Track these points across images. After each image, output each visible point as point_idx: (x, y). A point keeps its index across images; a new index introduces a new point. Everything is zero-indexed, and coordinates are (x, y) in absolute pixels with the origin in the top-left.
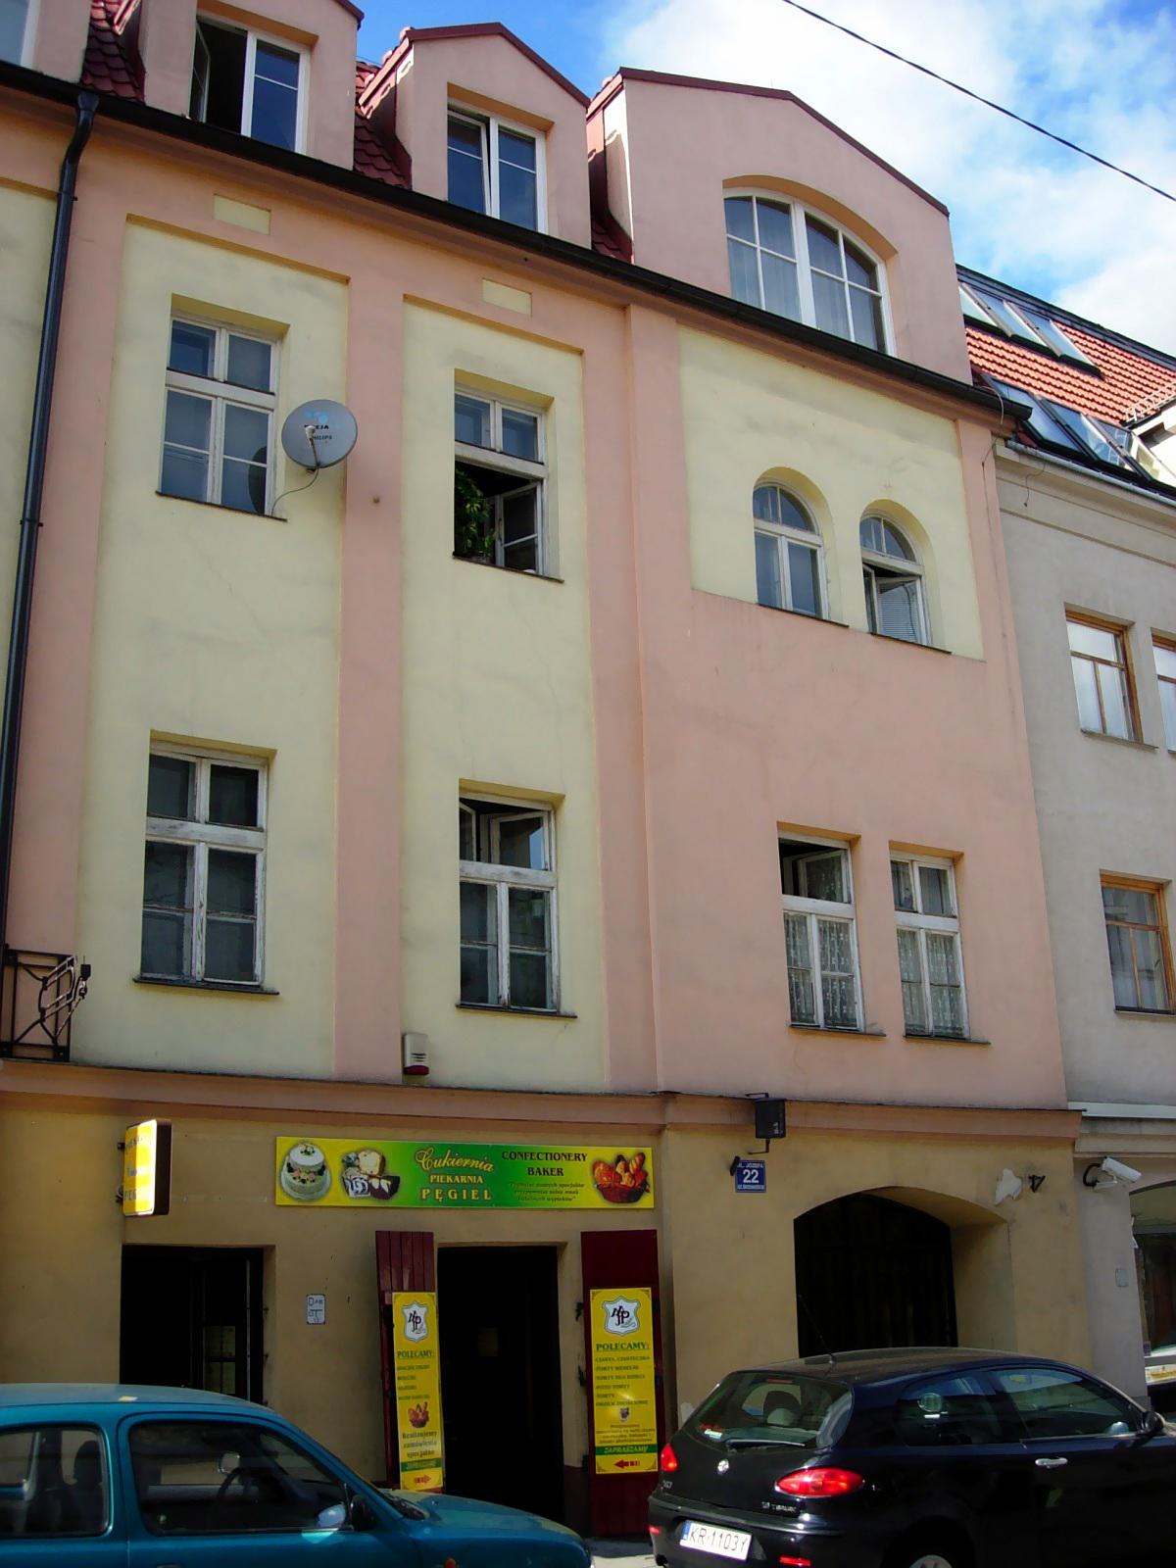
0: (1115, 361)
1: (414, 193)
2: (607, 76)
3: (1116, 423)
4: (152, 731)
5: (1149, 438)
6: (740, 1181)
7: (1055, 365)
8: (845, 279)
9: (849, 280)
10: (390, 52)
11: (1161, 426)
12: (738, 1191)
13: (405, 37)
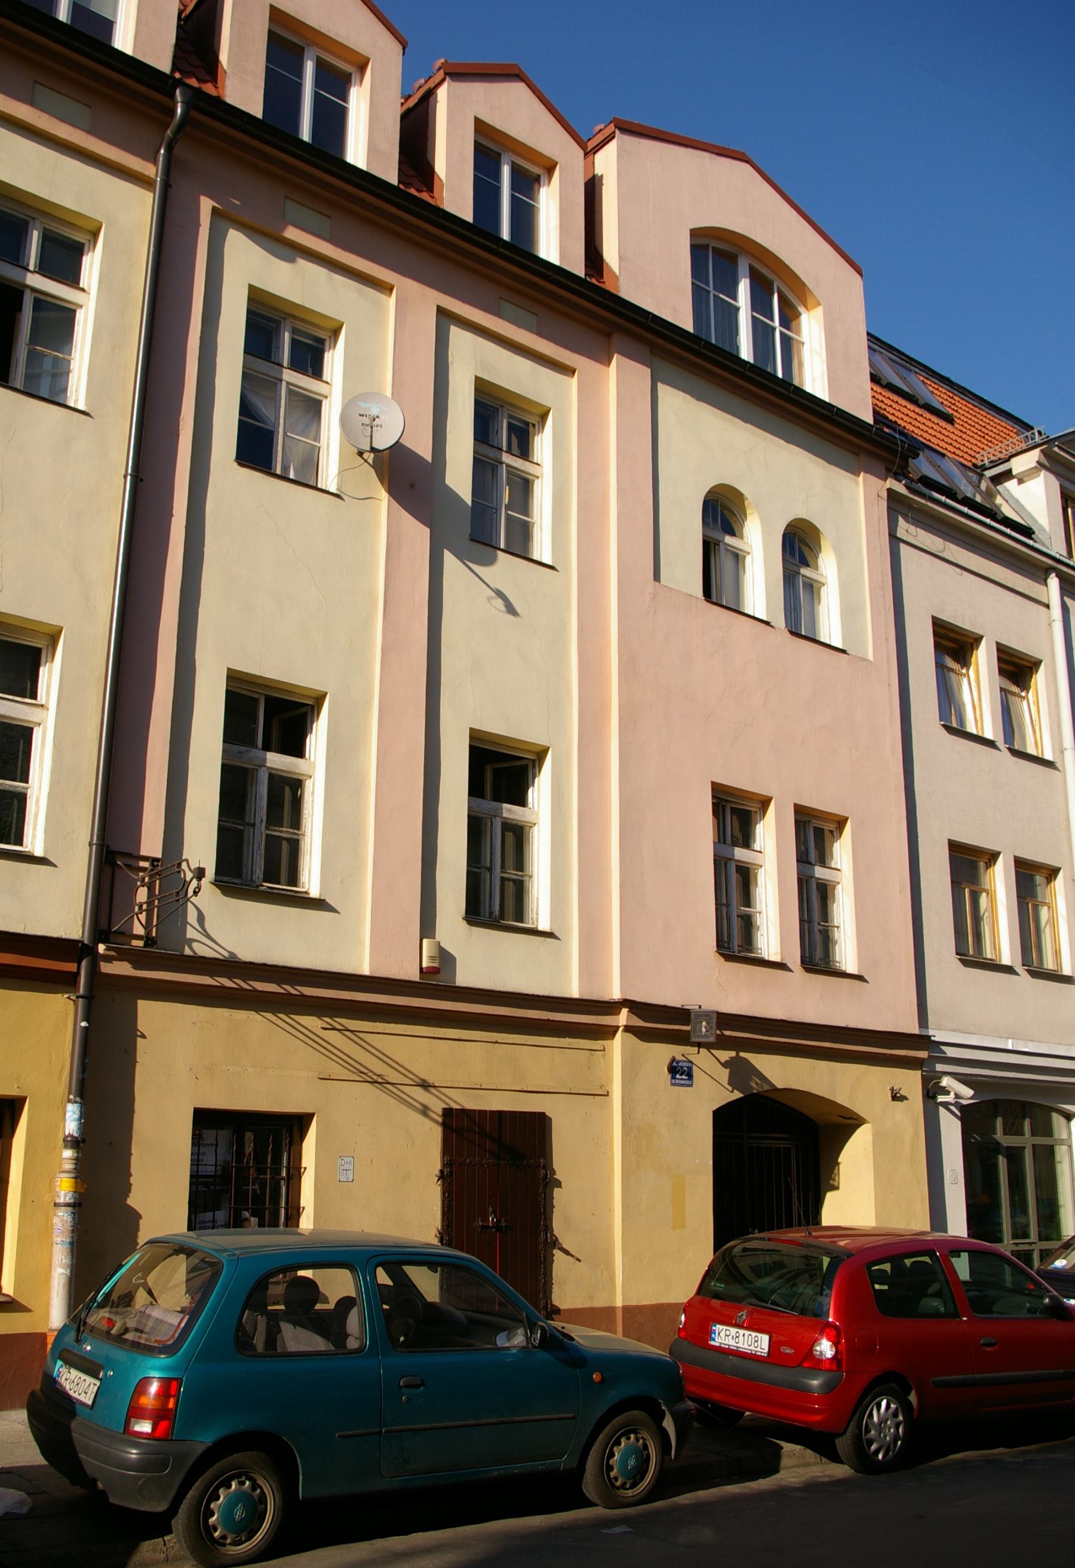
0: (960, 408)
1: (346, 163)
2: (601, 123)
3: (969, 464)
4: (229, 669)
5: (998, 479)
6: (673, 1077)
7: (917, 410)
8: (711, 288)
9: (781, 325)
10: (423, 81)
11: (1010, 471)
12: (672, 1084)
13: (440, 68)
